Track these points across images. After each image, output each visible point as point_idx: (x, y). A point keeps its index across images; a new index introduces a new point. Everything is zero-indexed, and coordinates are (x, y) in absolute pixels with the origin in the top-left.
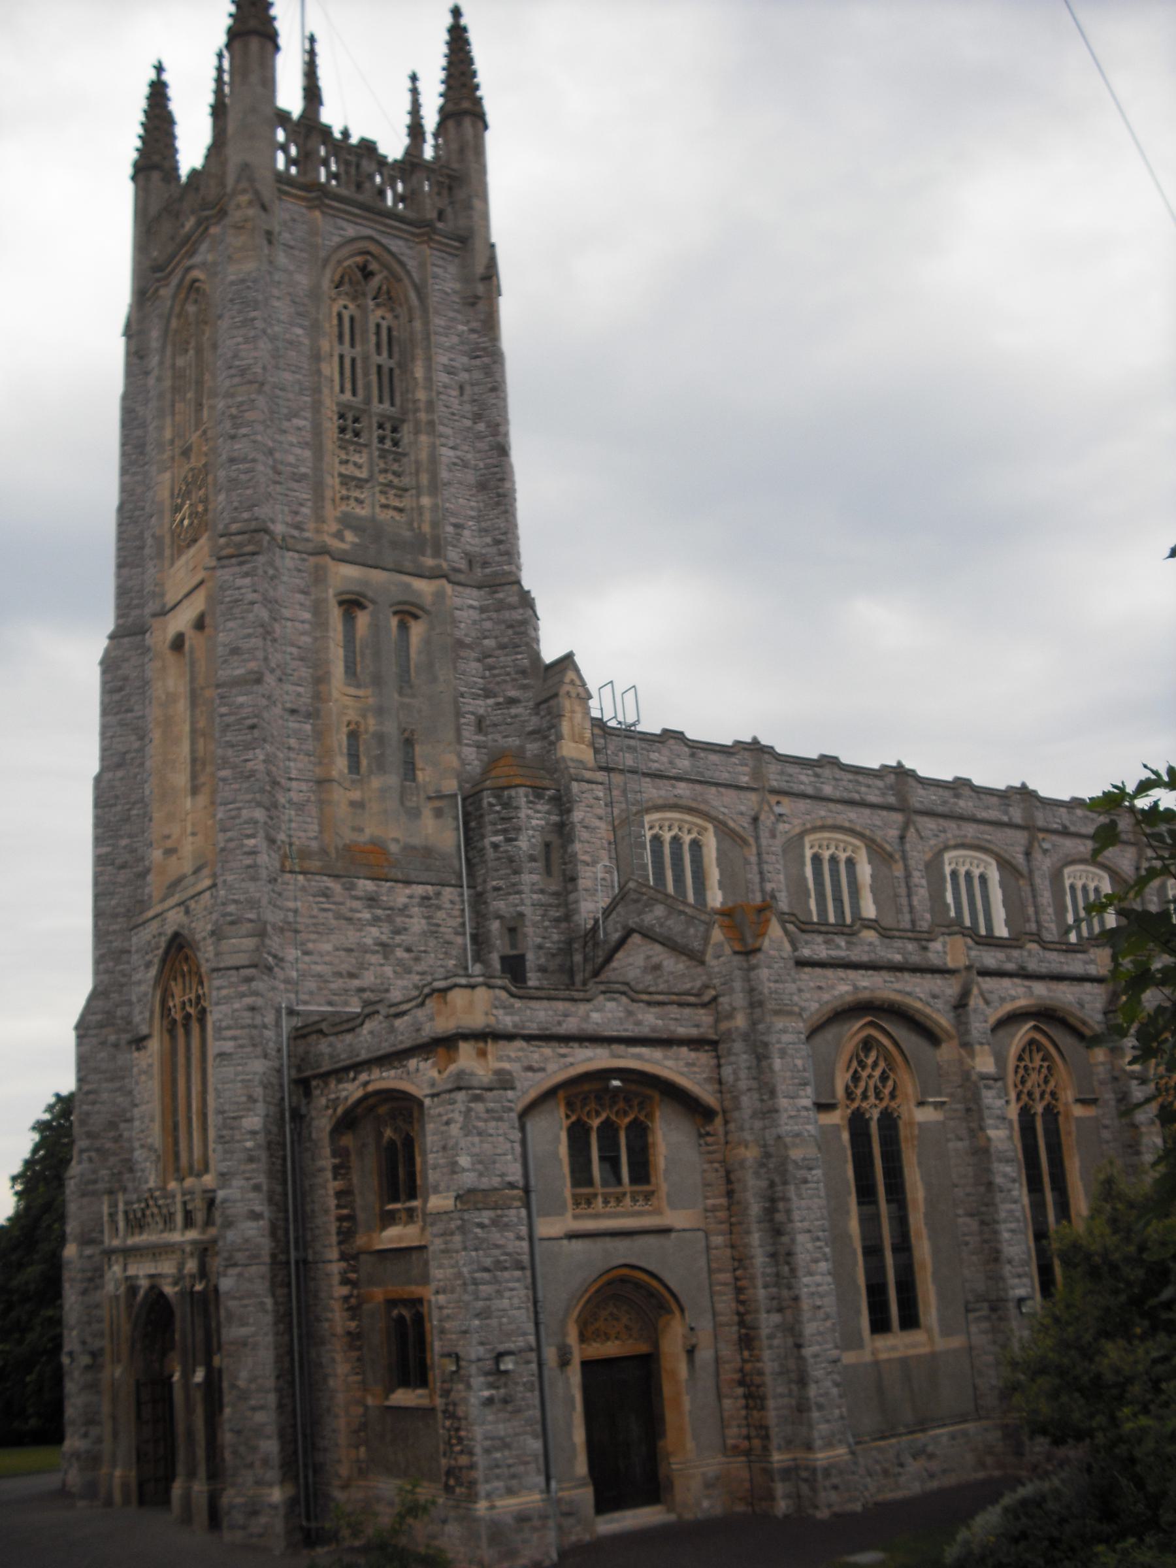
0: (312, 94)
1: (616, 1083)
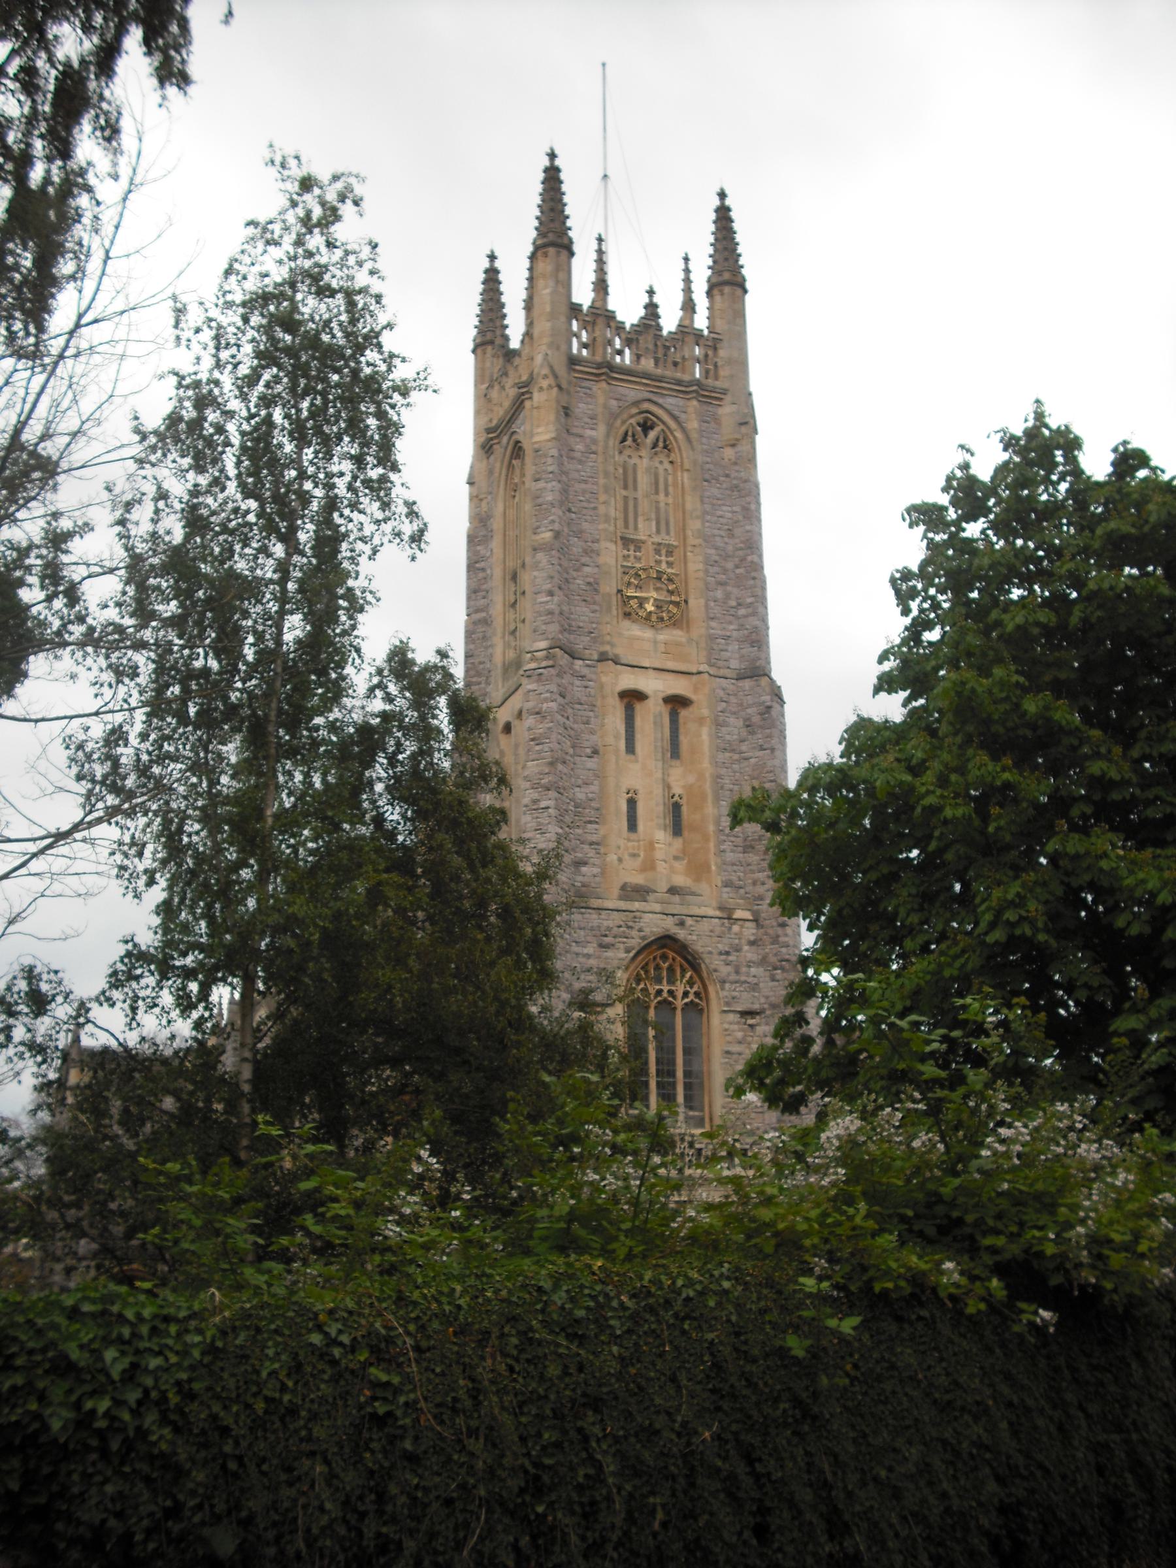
0: (601, 286)
1: (957, 887)
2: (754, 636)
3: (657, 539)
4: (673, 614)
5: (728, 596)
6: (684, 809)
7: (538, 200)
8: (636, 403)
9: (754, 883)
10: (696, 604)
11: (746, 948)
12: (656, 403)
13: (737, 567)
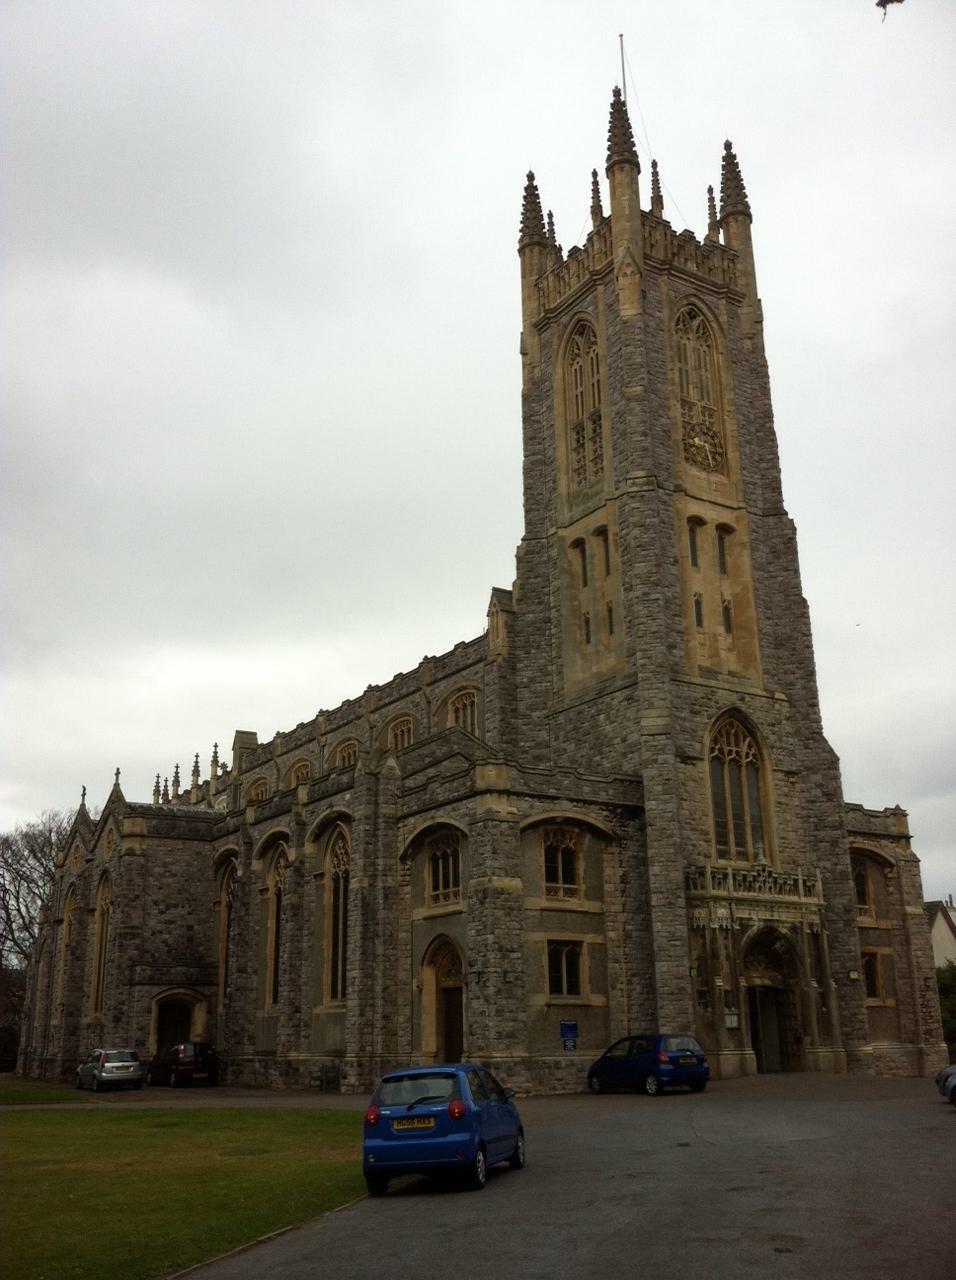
0: (657, 200)
2: (774, 484)
3: (703, 404)
4: (719, 465)
5: (753, 452)
6: (732, 611)
7: (608, 126)
8: (687, 297)
9: (786, 673)
10: (733, 455)
11: (784, 722)
12: (699, 298)
13: (758, 431)
